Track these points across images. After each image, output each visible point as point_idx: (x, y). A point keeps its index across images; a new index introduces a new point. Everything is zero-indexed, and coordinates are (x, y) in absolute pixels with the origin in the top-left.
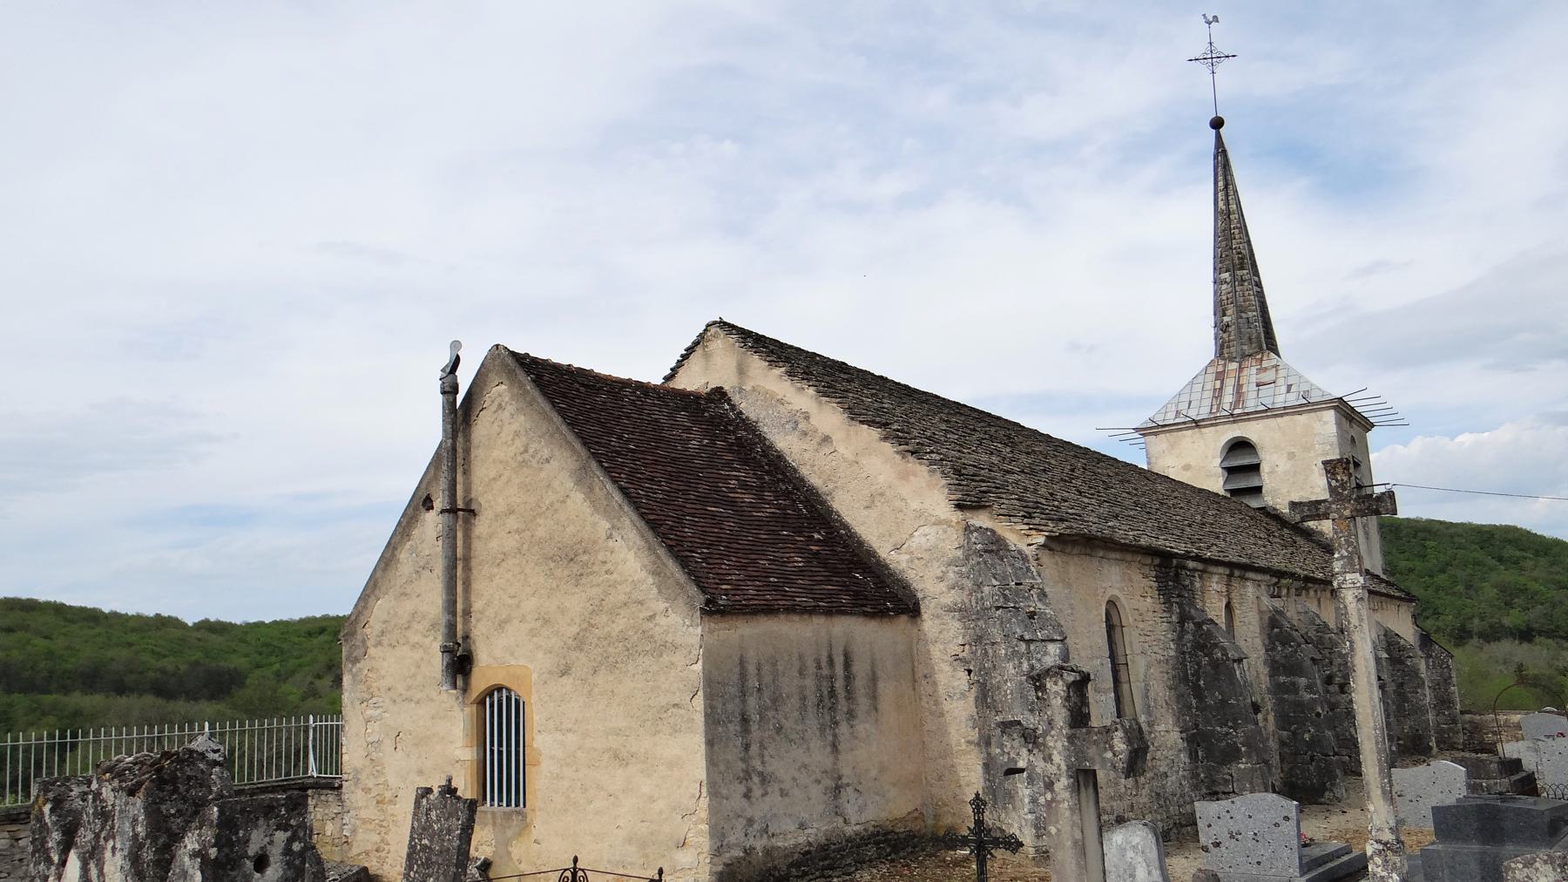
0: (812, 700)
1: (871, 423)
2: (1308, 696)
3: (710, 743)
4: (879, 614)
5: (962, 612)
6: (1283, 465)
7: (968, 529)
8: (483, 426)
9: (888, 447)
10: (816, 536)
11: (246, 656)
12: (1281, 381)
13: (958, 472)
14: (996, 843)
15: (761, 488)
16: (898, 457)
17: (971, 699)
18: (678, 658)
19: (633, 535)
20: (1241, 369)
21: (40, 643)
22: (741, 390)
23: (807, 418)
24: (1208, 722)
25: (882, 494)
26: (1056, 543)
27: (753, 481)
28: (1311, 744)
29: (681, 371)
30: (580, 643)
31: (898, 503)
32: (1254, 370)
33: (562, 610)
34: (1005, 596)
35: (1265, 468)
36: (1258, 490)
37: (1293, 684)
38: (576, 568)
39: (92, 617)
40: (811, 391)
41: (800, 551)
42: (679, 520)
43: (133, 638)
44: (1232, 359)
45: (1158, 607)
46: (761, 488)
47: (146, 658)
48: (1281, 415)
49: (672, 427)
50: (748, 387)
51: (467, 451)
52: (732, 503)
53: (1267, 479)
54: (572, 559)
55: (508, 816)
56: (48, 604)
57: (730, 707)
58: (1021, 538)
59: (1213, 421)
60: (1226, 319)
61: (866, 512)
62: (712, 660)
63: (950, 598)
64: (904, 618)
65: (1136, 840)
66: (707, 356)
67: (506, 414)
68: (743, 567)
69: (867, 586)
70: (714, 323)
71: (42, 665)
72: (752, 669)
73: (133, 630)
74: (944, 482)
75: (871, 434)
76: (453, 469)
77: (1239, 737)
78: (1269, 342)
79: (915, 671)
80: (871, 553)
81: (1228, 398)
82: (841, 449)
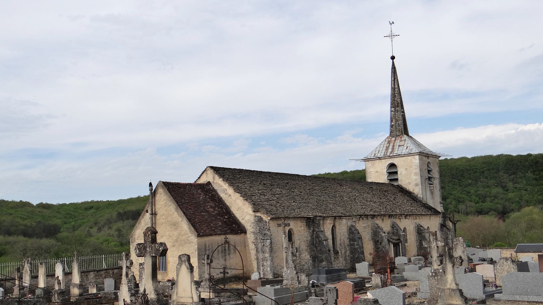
1: (238, 193)
3: (198, 259)
4: (236, 233)
5: (254, 233)
6: (404, 172)
7: (255, 216)
11: (60, 219)
12: (405, 145)
13: (254, 204)
18: (193, 244)
19: (185, 221)
27: (213, 205)
30: (176, 241)
33: (173, 235)
35: (399, 172)
36: (397, 180)
38: (176, 227)
41: (221, 221)
42: (195, 218)
43: (12, 211)
44: (393, 137)
46: (215, 207)
47: (18, 220)
49: (197, 194)
51: (155, 202)
52: (208, 211)
53: (399, 176)
54: (175, 225)
55: (164, 273)
60: (393, 123)
62: (199, 244)
63: (252, 230)
64: (243, 234)
66: (207, 174)
68: (207, 226)
69: (235, 227)
72: (207, 246)
73: (12, 208)
75: (238, 195)
77: (324, 257)
79: (245, 245)
80: (238, 220)
81: (390, 150)
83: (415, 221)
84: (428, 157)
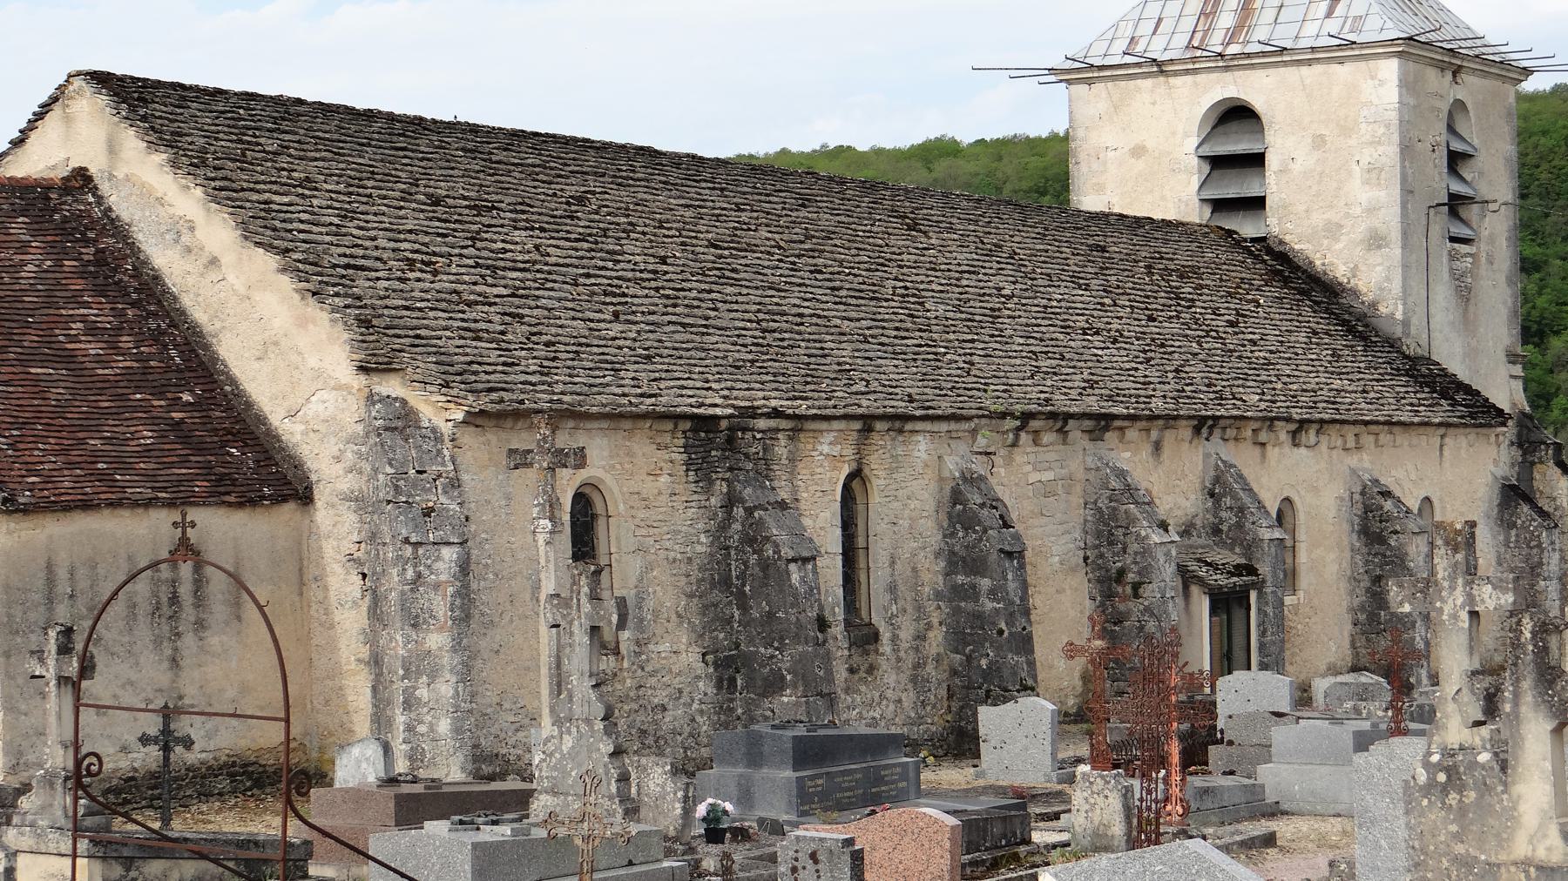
0: (144, 608)
1: (269, 247)
2: (989, 606)
4: (249, 501)
5: (359, 502)
6: (1305, 160)
7: (371, 399)
9: (286, 282)
10: (187, 397)
14: (178, 741)
15: (118, 331)
16: (297, 297)
17: (365, 609)
22: (111, 177)
23: (192, 229)
24: (751, 641)
25: (276, 344)
28: (987, 675)
29: (33, 135)
31: (294, 358)
34: (397, 487)
35: (1272, 161)
37: (974, 587)
40: (199, 192)
41: (153, 421)
45: (679, 488)
46: (118, 331)
48: (1309, 62)
50: (120, 174)
52: (67, 359)
53: (1274, 184)
57: (32, 616)
58: (437, 412)
61: (256, 365)
63: (347, 483)
65: (369, 752)
66: (68, 119)
68: (64, 451)
70: (79, 74)
72: (62, 574)
74: (346, 336)
75: (267, 262)
79: (301, 571)
80: (261, 420)
82: (231, 278)
83: (1353, 460)
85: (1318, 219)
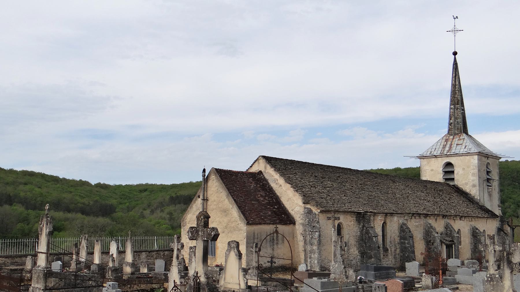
1: (289, 183)
3: (247, 247)
4: (285, 224)
5: (303, 224)
7: (305, 208)
8: (210, 183)
12: (464, 144)
15: (266, 196)
18: (242, 232)
19: (236, 209)
20: (453, 138)
21: (37, 189)
26: (322, 212)
27: (264, 195)
28: (407, 257)
32: (457, 140)
33: (223, 221)
35: (455, 172)
36: (453, 179)
38: (226, 214)
39: (55, 179)
41: (271, 211)
43: (72, 190)
44: (451, 135)
46: (266, 196)
47: (77, 198)
51: (207, 188)
52: (258, 200)
53: (456, 176)
54: (225, 212)
56: (39, 173)
58: (316, 210)
59: (441, 156)
60: (451, 121)
63: (301, 221)
64: (292, 225)
66: (259, 163)
67: (214, 182)
68: (257, 215)
69: (284, 217)
71: (39, 199)
72: (256, 234)
73: (72, 186)
75: (289, 186)
76: (204, 192)
77: (372, 253)
78: (465, 130)
80: (288, 211)
83: (471, 223)
84: (488, 158)
85: (464, 182)
